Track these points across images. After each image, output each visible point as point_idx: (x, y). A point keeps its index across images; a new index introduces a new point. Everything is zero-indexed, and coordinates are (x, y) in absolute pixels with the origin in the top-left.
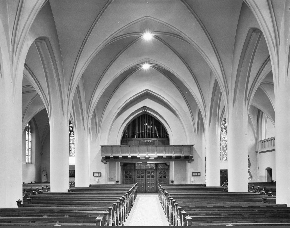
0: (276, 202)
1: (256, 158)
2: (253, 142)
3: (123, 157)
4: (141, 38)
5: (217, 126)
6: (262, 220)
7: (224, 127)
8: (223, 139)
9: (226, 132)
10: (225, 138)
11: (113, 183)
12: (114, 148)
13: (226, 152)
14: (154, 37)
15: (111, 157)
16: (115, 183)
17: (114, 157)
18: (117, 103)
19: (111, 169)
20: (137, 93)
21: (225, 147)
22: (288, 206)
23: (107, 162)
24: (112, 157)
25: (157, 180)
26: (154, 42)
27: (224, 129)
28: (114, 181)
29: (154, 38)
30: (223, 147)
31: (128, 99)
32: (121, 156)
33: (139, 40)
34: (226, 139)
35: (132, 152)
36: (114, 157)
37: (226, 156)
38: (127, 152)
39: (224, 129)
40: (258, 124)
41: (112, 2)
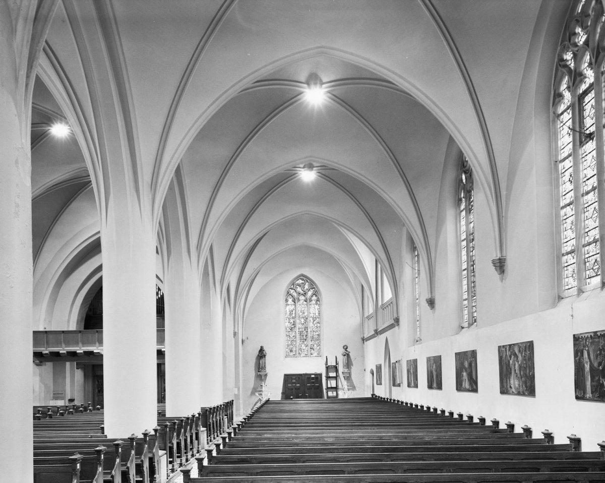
0: (165, 414)
1: (363, 348)
2: (357, 320)
3: (85, 352)
4: (299, 100)
5: (211, 292)
6: (406, 467)
7: (302, 292)
8: (301, 314)
9: (306, 301)
10: (304, 313)
11: (60, 403)
12: (51, 336)
13: (306, 340)
14: (330, 98)
15: (44, 352)
16: (65, 403)
17: (67, 352)
18: (61, 249)
19: (58, 375)
20: (93, 233)
21: (305, 330)
22: (589, 446)
23: (41, 362)
24: (46, 354)
25: (160, 397)
26: (329, 110)
27: (302, 294)
28: (63, 398)
29: (330, 100)
30: (301, 330)
31: (78, 246)
32: (80, 350)
33: (295, 104)
34: (306, 314)
35: (86, 344)
36: (67, 352)
37: (306, 346)
38: (77, 344)
39: (302, 294)
40: (433, 286)
41: (217, 31)
